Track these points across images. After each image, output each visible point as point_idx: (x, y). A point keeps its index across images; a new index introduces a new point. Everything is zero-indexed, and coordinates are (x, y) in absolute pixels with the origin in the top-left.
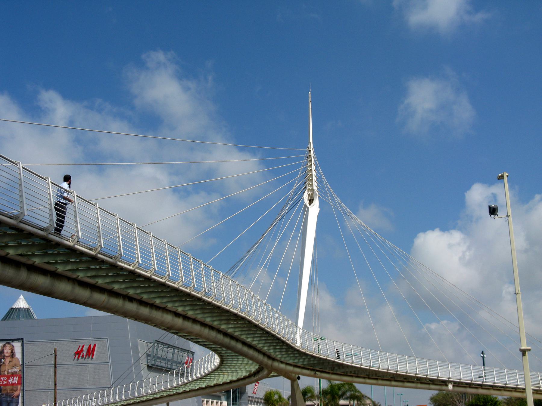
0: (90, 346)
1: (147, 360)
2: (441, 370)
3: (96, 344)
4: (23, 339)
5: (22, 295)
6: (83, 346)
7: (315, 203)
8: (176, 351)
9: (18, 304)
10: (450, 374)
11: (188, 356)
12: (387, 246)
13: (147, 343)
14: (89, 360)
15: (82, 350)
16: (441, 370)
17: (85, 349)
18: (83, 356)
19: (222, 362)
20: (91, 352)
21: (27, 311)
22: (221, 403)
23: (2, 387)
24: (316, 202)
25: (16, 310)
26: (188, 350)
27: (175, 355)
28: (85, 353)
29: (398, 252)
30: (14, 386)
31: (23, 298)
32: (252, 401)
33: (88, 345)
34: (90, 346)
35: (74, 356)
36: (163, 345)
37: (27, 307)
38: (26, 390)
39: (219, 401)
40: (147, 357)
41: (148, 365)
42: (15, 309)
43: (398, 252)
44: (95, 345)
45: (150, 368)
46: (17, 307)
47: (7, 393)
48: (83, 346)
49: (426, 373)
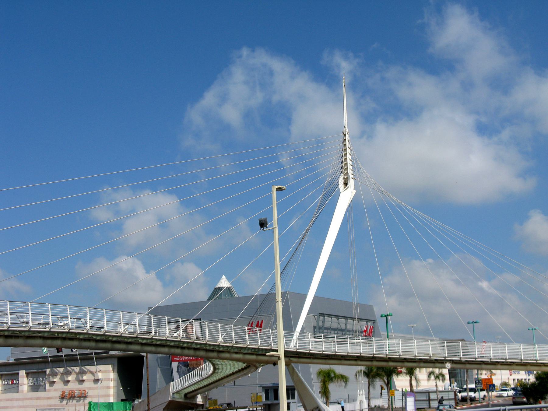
0: (258, 322)
2: (432, 345)
3: (263, 321)
4: (200, 319)
5: (224, 275)
7: (350, 184)
8: (350, 321)
9: (220, 284)
10: (534, 339)
12: (422, 221)
13: (314, 316)
16: (432, 345)
21: (229, 289)
23: (189, 362)
24: (351, 183)
25: (219, 289)
26: (374, 320)
27: (348, 325)
29: (437, 227)
30: (198, 361)
31: (225, 278)
34: (258, 322)
36: (332, 317)
37: (229, 286)
42: (218, 289)
43: (437, 227)
46: (219, 286)
47: (193, 367)
49: (372, 352)
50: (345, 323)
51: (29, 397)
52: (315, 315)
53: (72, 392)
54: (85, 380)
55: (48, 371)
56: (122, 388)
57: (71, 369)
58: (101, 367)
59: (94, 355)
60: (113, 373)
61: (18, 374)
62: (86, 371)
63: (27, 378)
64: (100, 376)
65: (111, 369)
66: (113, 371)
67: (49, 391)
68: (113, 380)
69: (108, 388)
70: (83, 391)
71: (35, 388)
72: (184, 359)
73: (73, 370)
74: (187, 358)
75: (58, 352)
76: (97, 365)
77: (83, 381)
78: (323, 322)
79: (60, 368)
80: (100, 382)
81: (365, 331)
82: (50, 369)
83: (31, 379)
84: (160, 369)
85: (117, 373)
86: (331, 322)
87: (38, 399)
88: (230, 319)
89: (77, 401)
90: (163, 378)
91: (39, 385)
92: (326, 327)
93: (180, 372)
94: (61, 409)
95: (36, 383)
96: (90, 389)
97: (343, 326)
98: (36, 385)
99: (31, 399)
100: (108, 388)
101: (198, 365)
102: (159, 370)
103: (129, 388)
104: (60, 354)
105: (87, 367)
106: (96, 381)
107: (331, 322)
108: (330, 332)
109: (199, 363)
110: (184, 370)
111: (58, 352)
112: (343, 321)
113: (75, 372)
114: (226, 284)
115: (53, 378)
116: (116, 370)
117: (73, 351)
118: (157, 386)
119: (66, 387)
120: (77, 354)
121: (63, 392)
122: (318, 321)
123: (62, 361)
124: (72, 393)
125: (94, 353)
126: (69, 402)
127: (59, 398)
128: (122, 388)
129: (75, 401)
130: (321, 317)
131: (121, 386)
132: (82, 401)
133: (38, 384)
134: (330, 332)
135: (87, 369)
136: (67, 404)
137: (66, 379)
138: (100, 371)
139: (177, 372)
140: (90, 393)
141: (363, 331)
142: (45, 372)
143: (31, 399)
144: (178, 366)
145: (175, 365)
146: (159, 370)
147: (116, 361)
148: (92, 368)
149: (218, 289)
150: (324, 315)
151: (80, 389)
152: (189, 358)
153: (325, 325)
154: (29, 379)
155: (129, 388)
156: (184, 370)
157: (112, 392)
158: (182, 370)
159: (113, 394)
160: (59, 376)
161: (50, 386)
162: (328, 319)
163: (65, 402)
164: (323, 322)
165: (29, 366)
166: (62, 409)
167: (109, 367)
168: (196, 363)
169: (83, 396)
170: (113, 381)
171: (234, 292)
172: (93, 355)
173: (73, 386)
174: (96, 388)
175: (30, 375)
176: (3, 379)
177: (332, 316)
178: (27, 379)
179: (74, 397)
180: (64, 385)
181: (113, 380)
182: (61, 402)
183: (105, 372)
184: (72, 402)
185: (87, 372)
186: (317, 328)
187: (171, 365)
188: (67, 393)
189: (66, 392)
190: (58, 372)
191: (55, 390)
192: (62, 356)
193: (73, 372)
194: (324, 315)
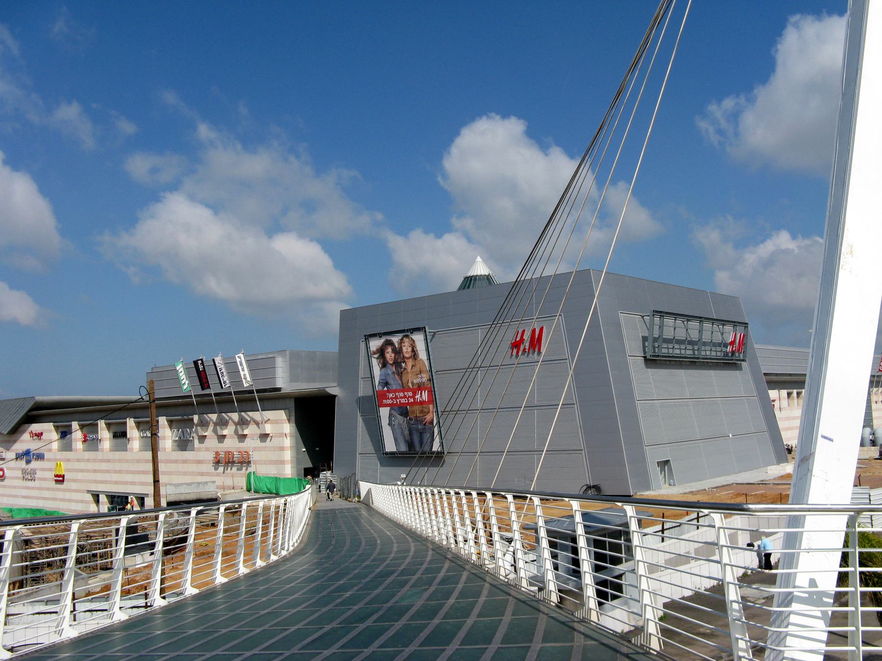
0: (534, 331)
13: (643, 317)
15: (522, 340)
17: (527, 337)
18: (524, 350)
20: (536, 342)
30: (424, 406)
31: (481, 261)
34: (534, 331)
37: (487, 274)
42: (469, 279)
44: (541, 329)
45: (652, 361)
50: (698, 328)
51: (173, 458)
52: (644, 314)
53: (228, 453)
54: (247, 435)
55: (196, 418)
56: (304, 450)
57: (228, 416)
58: (269, 414)
59: (257, 393)
60: (288, 424)
61: (126, 423)
62: (249, 419)
63: (169, 429)
64: (268, 428)
65: (285, 417)
66: (289, 421)
67: (199, 450)
68: (288, 435)
69: (282, 449)
70: (244, 453)
71: (183, 444)
72: (400, 401)
73: (252, 418)
74: (406, 400)
75: (203, 389)
76: (262, 410)
77: (245, 436)
78: (661, 327)
79: (232, 413)
80: (269, 439)
81: (732, 343)
82: (217, 415)
83: (175, 430)
84: (362, 418)
85: (294, 425)
86: (712, 332)
87: (185, 462)
88: (482, 327)
89: (238, 469)
90: (367, 435)
91: (186, 440)
92: (716, 341)
93: (394, 425)
94: (208, 483)
95: (182, 438)
96: (255, 449)
97: (694, 335)
98: (183, 440)
99: (176, 461)
100: (282, 449)
101: (425, 413)
102: (361, 420)
103: (317, 449)
104: (207, 392)
105: (250, 413)
106: (264, 437)
107: (712, 332)
108: (684, 348)
109: (426, 410)
110: (401, 422)
111: (203, 389)
112: (694, 324)
113: (233, 422)
114: (482, 270)
115: (222, 429)
116: (293, 418)
117: (223, 386)
118: (358, 449)
119: (221, 445)
120: (253, 390)
121: (217, 453)
122: (650, 329)
123: (212, 403)
124: (230, 456)
125: (214, 394)
126: (227, 470)
127: (213, 463)
128: (304, 450)
129: (234, 469)
130: (657, 319)
131: (303, 445)
132: (244, 468)
133: (185, 438)
134: (711, 350)
135: (249, 416)
136: (224, 472)
137: (220, 433)
138: (267, 421)
139: (389, 424)
140: (255, 456)
141: (729, 342)
142: (192, 419)
143: (176, 461)
144: (391, 415)
145: (384, 412)
146: (360, 420)
147: (292, 404)
148: (256, 415)
149: (469, 279)
150: (662, 314)
151: (239, 450)
152: (408, 401)
153: (664, 333)
154: (172, 430)
155: (317, 449)
156: (401, 422)
157: (288, 455)
158: (397, 421)
159: (290, 459)
160: (211, 428)
161: (200, 443)
162: (669, 321)
163: (221, 469)
164: (661, 327)
165: (172, 410)
166: (211, 483)
167: (281, 415)
168: (420, 409)
169: (245, 462)
170: (289, 438)
171: (494, 280)
172: (212, 397)
173: (231, 444)
174: (264, 449)
175: (174, 425)
176: (141, 428)
177: (676, 315)
178: (171, 430)
179: (233, 462)
180: (219, 442)
181: (288, 435)
182: (216, 469)
183: (276, 422)
184: (231, 469)
185: (250, 421)
186: (650, 340)
187: (378, 412)
188: (222, 455)
189: (221, 453)
190: (228, 419)
191: (207, 449)
192: (210, 395)
193: (230, 421)
194: (662, 314)
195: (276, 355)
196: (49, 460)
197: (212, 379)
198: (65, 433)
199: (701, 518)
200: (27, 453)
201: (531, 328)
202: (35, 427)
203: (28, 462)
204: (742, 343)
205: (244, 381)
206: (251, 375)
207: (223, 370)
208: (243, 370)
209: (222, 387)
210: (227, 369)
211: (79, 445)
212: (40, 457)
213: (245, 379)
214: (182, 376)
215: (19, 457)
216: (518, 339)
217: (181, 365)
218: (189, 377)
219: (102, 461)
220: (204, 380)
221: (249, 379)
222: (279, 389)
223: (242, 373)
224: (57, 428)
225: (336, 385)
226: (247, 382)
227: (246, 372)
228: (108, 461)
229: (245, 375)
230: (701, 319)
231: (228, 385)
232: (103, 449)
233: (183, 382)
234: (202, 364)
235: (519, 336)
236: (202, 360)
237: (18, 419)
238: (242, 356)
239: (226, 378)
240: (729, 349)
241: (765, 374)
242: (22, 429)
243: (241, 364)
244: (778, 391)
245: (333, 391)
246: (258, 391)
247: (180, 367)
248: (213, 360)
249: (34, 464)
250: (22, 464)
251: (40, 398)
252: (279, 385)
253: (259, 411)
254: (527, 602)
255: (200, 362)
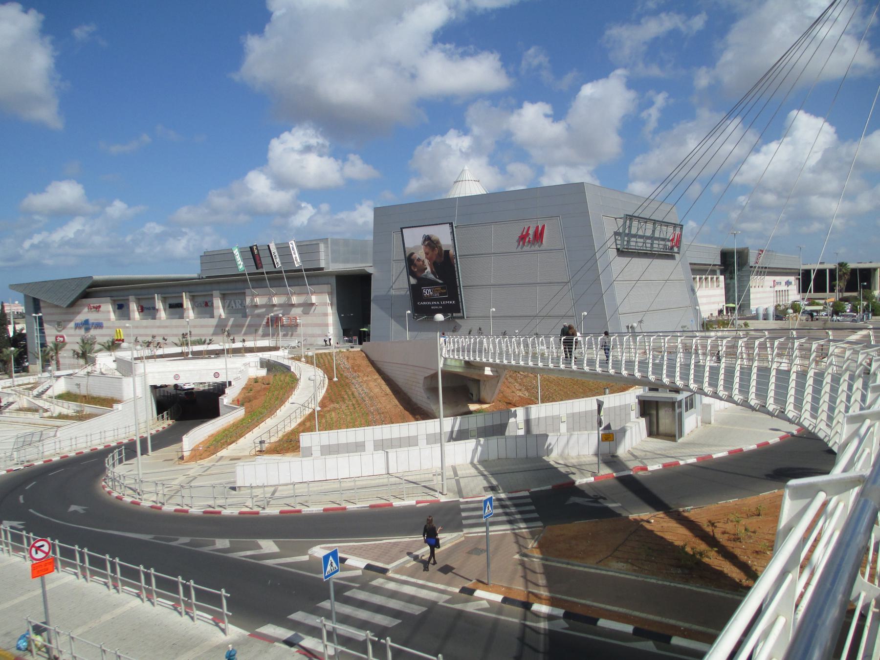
0: (537, 227)
1: (616, 240)
6: (529, 228)
11: (674, 230)
14: (536, 247)
15: (527, 234)
17: (531, 232)
18: (529, 241)
19: (822, 491)
20: (539, 236)
22: (717, 278)
28: (531, 236)
32: (761, 272)
33: (535, 226)
34: (537, 227)
35: (517, 244)
38: (447, 479)
39: (715, 277)
40: (615, 237)
41: (618, 250)
44: (543, 227)
45: (621, 252)
48: (529, 228)
81: (673, 240)
111: (257, 269)
147: (333, 281)
192: (263, 273)
195: (318, 242)
196: (107, 328)
197: (265, 261)
198: (121, 308)
199: (452, 574)
200: (86, 322)
201: (536, 225)
202: (93, 302)
203: (87, 330)
204: (679, 241)
205: (295, 262)
206: (301, 258)
207: (276, 254)
208: (295, 254)
209: (275, 267)
210: (278, 253)
211: (136, 315)
212: (99, 326)
213: (297, 260)
214: (238, 258)
215: (77, 326)
216: (524, 233)
217: (237, 250)
218: (244, 260)
219: (159, 327)
220: (258, 262)
221: (299, 261)
222: (322, 269)
223: (294, 256)
224: (114, 302)
225: (371, 265)
226: (298, 263)
227: (297, 255)
228: (166, 327)
229: (296, 257)
230: (655, 222)
231: (280, 266)
232: (134, 318)
233: (239, 263)
234: (257, 248)
235: (526, 230)
236: (256, 245)
237: (77, 295)
238: (293, 242)
239: (278, 260)
240: (669, 244)
241: (691, 264)
242: (79, 302)
243: (293, 248)
244: (544, 585)
245: (370, 270)
246: (306, 270)
247: (236, 252)
248: (268, 246)
249: (93, 332)
250: (82, 332)
251: (97, 277)
252: (322, 265)
253: (268, 287)
254: (213, 623)
255: (255, 247)
